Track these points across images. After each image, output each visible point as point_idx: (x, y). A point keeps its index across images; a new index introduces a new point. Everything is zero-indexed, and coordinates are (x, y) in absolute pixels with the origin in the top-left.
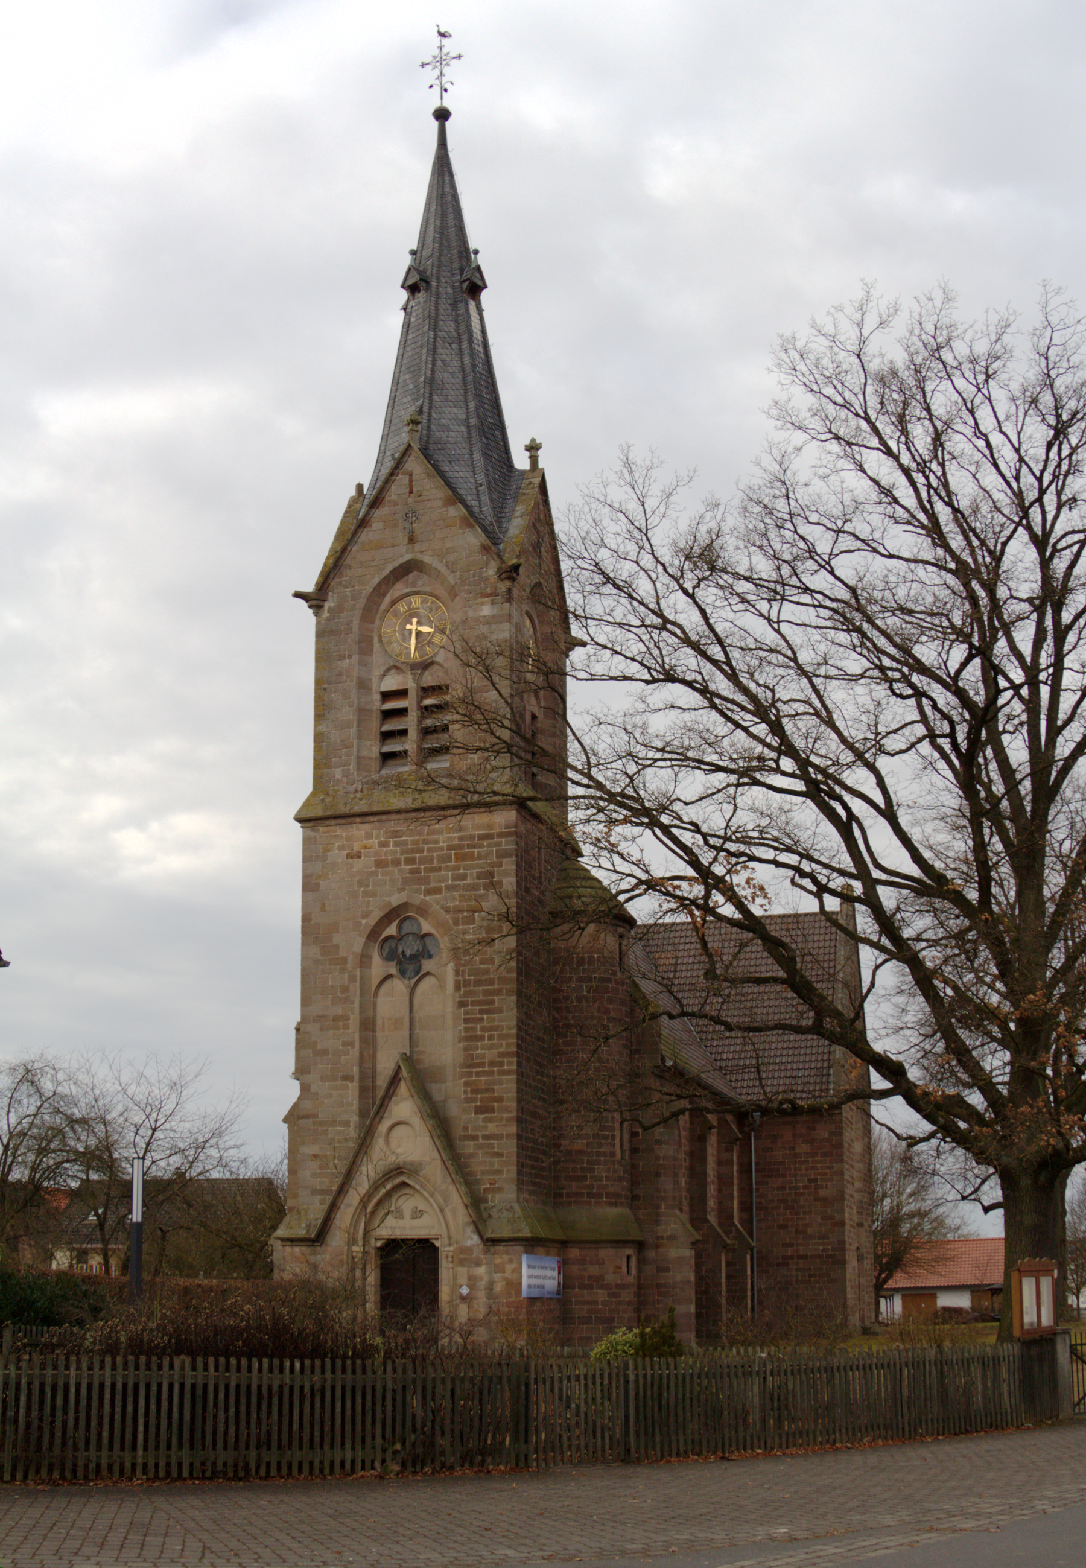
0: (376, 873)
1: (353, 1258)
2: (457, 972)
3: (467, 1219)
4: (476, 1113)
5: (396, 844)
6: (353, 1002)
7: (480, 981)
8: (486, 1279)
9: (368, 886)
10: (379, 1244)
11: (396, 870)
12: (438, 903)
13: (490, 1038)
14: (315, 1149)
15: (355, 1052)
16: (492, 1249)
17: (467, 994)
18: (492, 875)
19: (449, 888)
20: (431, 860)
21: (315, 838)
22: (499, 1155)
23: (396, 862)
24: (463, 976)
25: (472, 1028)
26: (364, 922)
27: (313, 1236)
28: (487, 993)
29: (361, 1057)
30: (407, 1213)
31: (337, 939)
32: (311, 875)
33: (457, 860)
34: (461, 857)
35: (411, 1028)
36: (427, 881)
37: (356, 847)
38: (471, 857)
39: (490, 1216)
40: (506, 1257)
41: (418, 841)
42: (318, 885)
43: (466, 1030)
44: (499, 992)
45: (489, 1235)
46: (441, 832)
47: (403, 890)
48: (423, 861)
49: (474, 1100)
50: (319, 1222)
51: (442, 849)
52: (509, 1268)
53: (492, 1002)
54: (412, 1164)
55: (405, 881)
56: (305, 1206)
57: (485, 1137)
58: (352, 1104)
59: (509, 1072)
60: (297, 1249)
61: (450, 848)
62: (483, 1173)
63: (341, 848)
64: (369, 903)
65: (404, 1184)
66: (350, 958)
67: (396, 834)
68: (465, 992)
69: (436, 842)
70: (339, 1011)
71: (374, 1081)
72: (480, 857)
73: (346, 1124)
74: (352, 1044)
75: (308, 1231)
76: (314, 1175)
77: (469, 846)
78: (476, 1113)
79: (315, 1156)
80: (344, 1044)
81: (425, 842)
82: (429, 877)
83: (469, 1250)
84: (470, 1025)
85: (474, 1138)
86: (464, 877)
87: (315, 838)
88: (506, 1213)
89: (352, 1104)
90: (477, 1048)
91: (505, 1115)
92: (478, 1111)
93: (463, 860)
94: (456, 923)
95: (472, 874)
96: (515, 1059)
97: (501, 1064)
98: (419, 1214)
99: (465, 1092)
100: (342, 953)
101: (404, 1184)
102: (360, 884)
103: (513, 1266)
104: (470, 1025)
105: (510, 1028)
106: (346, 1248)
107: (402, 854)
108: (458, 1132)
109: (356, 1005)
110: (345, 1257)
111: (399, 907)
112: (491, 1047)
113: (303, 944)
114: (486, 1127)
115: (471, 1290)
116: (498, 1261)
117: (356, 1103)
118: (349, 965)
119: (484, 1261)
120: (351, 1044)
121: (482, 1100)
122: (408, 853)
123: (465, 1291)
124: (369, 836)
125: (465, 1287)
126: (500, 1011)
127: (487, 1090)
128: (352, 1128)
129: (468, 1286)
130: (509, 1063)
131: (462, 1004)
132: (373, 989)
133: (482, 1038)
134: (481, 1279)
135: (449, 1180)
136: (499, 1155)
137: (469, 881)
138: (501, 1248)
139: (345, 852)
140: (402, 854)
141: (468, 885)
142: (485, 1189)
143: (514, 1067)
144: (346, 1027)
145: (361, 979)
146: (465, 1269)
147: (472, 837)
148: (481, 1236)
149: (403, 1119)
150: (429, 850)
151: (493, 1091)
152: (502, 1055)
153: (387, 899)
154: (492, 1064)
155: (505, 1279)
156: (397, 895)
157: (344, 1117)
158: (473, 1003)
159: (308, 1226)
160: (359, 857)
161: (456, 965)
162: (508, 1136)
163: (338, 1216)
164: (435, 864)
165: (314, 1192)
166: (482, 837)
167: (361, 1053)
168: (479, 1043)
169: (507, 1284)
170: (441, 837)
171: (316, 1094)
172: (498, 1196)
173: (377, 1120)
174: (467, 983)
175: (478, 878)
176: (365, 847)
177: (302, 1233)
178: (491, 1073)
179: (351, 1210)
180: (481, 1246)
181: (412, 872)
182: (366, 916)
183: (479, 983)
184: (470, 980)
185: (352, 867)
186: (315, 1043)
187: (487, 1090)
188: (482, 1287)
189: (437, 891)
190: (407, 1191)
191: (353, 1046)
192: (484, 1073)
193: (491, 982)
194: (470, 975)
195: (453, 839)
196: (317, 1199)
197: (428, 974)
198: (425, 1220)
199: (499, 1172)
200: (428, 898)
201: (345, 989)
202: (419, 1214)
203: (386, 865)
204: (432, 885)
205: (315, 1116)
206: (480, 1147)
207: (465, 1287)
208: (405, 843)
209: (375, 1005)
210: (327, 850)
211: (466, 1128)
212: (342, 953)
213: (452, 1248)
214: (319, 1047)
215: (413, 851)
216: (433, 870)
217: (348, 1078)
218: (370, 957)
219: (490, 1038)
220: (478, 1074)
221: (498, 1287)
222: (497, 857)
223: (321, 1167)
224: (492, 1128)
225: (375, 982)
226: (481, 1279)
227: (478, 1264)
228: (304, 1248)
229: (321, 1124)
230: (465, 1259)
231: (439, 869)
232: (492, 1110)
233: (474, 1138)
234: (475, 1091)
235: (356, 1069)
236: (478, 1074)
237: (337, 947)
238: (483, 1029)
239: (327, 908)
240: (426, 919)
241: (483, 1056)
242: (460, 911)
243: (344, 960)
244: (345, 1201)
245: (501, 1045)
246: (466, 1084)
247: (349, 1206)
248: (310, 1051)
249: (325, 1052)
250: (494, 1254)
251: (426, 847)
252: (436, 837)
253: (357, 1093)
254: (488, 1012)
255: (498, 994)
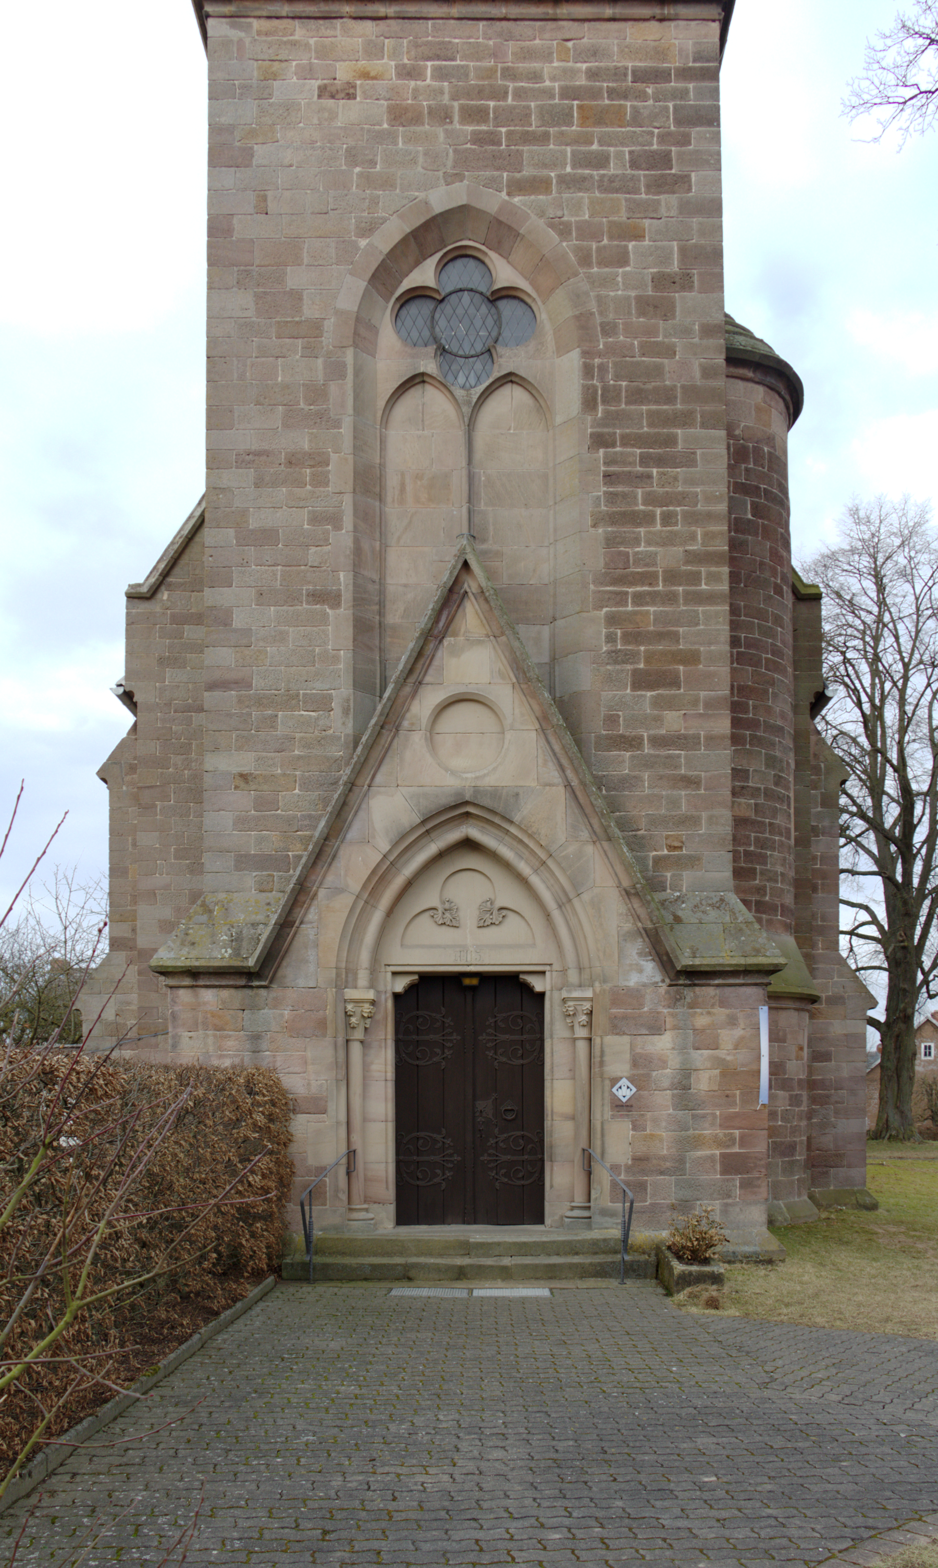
0: (390, 137)
1: (347, 1015)
2: (588, 371)
3: (628, 926)
4: (636, 686)
5: (440, 74)
6: (337, 424)
7: (639, 391)
8: (674, 1061)
9: (373, 163)
10: (400, 985)
11: (440, 132)
12: (541, 214)
13: (668, 519)
14: (245, 761)
15: (343, 538)
16: (689, 994)
17: (611, 418)
18: (665, 160)
19: (566, 182)
20: (525, 117)
21: (240, 41)
22: (690, 782)
23: (442, 115)
24: (602, 379)
25: (624, 496)
26: (363, 243)
27: (251, 962)
28: (655, 419)
29: (358, 550)
30: (469, 915)
31: (295, 278)
32: (230, 129)
33: (584, 120)
34: (600, 118)
35: (471, 498)
36: (514, 161)
37: (343, 72)
38: (617, 117)
39: (678, 920)
40: (721, 1013)
41: (493, 71)
42: (248, 153)
43: (612, 498)
44: (685, 419)
45: (685, 960)
46: (547, 56)
47: (459, 177)
48: (503, 117)
49: (629, 657)
50: (265, 933)
51: (549, 94)
52: (728, 1037)
53: (671, 441)
54: (495, 793)
55: (464, 161)
56: (222, 896)
57: (657, 742)
58: (336, 659)
59: (710, 598)
60: (209, 996)
61: (569, 93)
62: (654, 822)
63: (307, 73)
64: (375, 201)
65: (469, 845)
66: (329, 325)
67: (442, 53)
68: (607, 413)
69: (536, 77)
70: (303, 441)
71: (381, 613)
72: (637, 119)
73: (323, 703)
74: (335, 521)
75: (237, 953)
76: (242, 823)
77: (612, 93)
78: (636, 686)
79: (244, 777)
80: (315, 519)
81: (510, 74)
82: (520, 153)
83: (635, 996)
84: (620, 489)
85: (633, 743)
86: (601, 161)
87: (240, 41)
88: (713, 914)
89: (336, 659)
90: (637, 541)
91: (702, 694)
92: (641, 681)
93: (600, 122)
94: (585, 260)
95: (619, 155)
96: (725, 570)
97: (694, 578)
98: (496, 917)
99: (611, 638)
100: (309, 311)
101: (469, 845)
102: (352, 157)
103: (738, 1032)
104: (620, 489)
105: (709, 499)
106: (331, 993)
107: (454, 98)
108: (595, 728)
109: (346, 430)
110: (329, 1012)
111: (446, 216)
112: (668, 541)
113: (211, 287)
114: (658, 719)
115: (639, 1088)
116: (701, 1021)
117: (346, 657)
118: (328, 340)
119: (670, 1022)
120: (335, 521)
121: (649, 658)
122: (468, 96)
123: (624, 1092)
124: (373, 50)
125: (624, 1082)
126: (689, 460)
127: (660, 636)
128: (337, 713)
129: (631, 1080)
130: (713, 578)
131: (600, 441)
132: (381, 403)
133: (648, 519)
134: (664, 1064)
135: (585, 834)
136: (690, 782)
137: (613, 169)
138: (708, 992)
139: (315, 84)
140: (454, 98)
141: (612, 179)
142: (658, 860)
143: (725, 587)
144: (320, 480)
145: (357, 373)
146: (626, 1039)
147: (619, 74)
148: (665, 960)
149: (471, 689)
150: (519, 94)
151: (675, 637)
152: (693, 558)
153: (421, 195)
154: (672, 577)
155: (719, 1062)
156: (443, 189)
157: (318, 687)
158: (626, 441)
159: (236, 941)
160: (351, 96)
161: (585, 354)
162: (711, 740)
163: (312, 915)
164: (534, 126)
165: (243, 861)
166: (641, 76)
167: (357, 541)
168: (642, 530)
169: (723, 1074)
170: (547, 69)
171: (247, 632)
172: (688, 877)
173: (407, 689)
174: (610, 396)
175: (634, 164)
176: (366, 75)
177: (222, 956)
178: (671, 598)
179: (344, 903)
180: (663, 988)
181: (478, 139)
182: (368, 229)
183: (637, 396)
184: (618, 389)
185: (333, 116)
186: (244, 513)
187: (660, 636)
188: (666, 1083)
189: (538, 185)
190: (471, 860)
191: (338, 527)
192: (653, 598)
193: (668, 396)
194: (617, 377)
195: (573, 73)
196: (250, 879)
197: (509, 378)
198: (512, 929)
199: (690, 821)
200: (516, 200)
201: (317, 393)
202: (496, 917)
203: (417, 120)
204: (528, 172)
205: (243, 684)
206: (648, 763)
207: (624, 1082)
208: (463, 73)
209: (383, 441)
210: (270, 76)
211: (612, 720)
212: (309, 311)
213: (589, 994)
214: (253, 524)
215: (480, 93)
216: (528, 138)
217: (329, 598)
218: (374, 330)
219: (668, 519)
220: (639, 599)
221: (704, 1082)
222: (678, 122)
223: (260, 804)
224: (673, 721)
225: (386, 387)
226: (664, 1064)
227: (656, 1029)
228: (225, 993)
229: (260, 702)
230: (625, 1018)
231: (544, 138)
232: (675, 682)
233: (633, 743)
234: (634, 637)
235: (344, 578)
236: (639, 599)
237: (296, 296)
238: (650, 499)
239: (272, 206)
240: (506, 256)
241: (650, 559)
242: (596, 235)
243: (316, 327)
244: (330, 879)
245: (693, 537)
246: (612, 620)
247: (339, 891)
248: (231, 532)
249: (267, 536)
250: (692, 1006)
251: (511, 85)
252: (536, 65)
253: (348, 631)
254: (660, 461)
255: (684, 425)
